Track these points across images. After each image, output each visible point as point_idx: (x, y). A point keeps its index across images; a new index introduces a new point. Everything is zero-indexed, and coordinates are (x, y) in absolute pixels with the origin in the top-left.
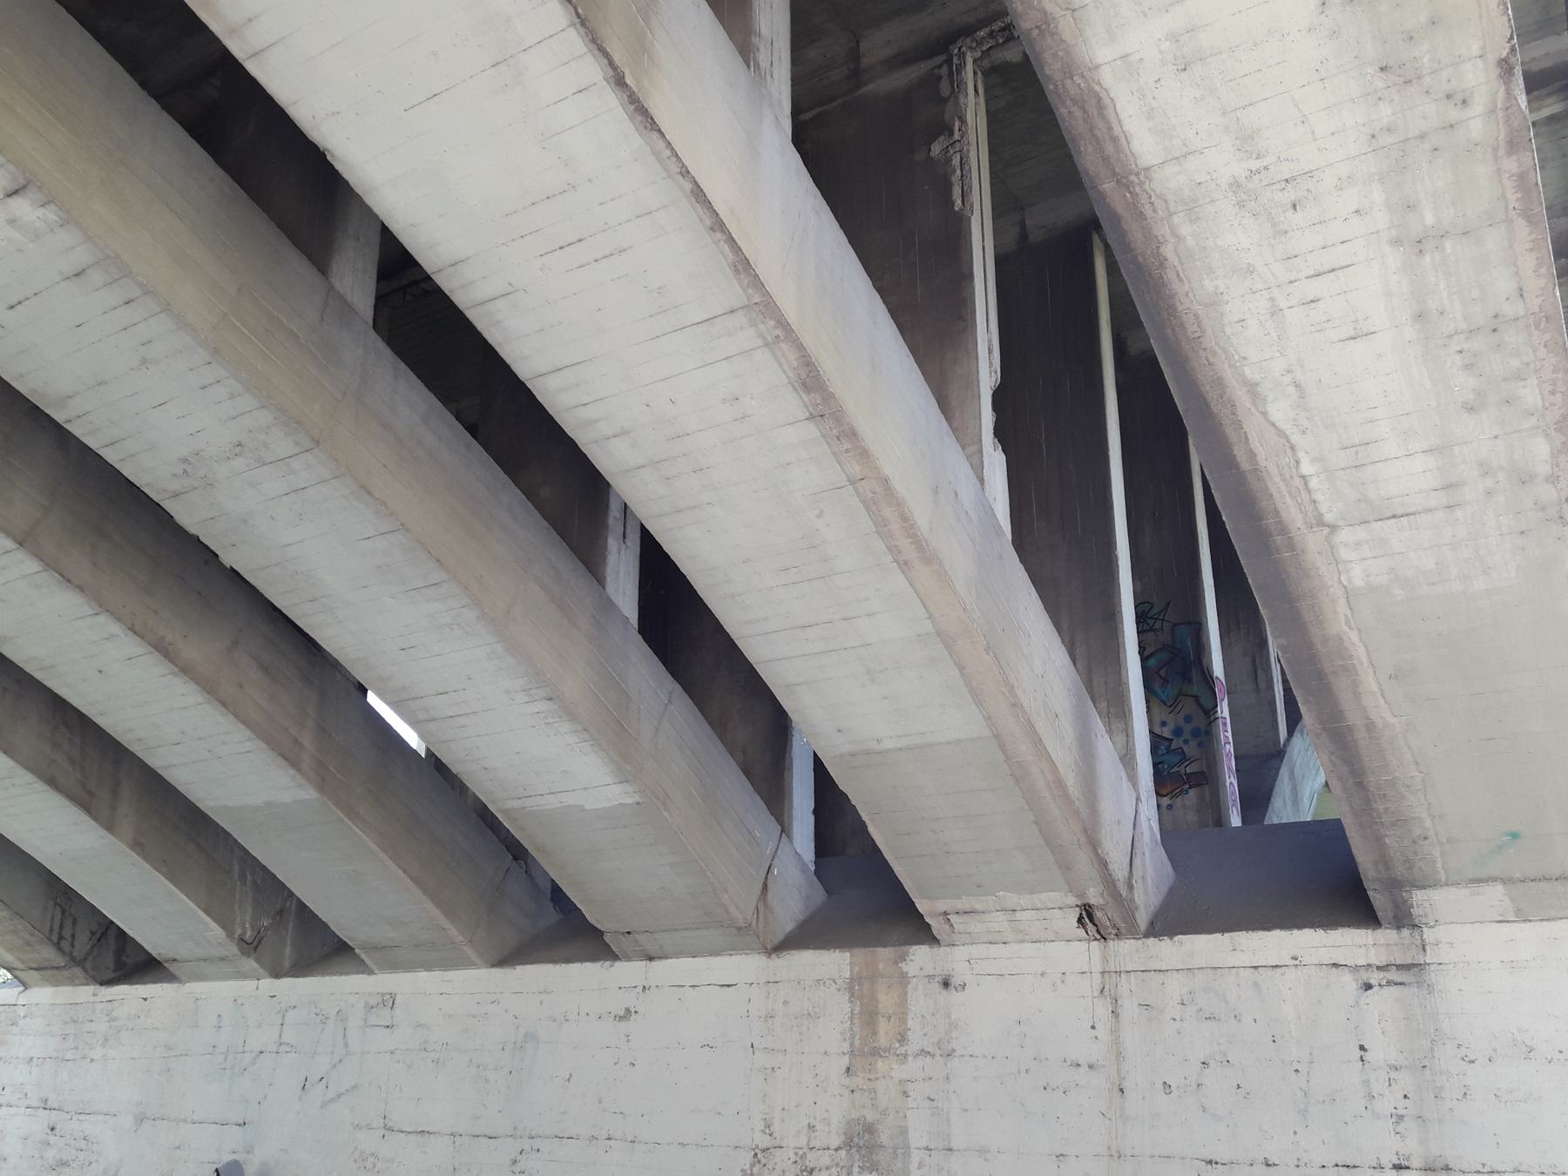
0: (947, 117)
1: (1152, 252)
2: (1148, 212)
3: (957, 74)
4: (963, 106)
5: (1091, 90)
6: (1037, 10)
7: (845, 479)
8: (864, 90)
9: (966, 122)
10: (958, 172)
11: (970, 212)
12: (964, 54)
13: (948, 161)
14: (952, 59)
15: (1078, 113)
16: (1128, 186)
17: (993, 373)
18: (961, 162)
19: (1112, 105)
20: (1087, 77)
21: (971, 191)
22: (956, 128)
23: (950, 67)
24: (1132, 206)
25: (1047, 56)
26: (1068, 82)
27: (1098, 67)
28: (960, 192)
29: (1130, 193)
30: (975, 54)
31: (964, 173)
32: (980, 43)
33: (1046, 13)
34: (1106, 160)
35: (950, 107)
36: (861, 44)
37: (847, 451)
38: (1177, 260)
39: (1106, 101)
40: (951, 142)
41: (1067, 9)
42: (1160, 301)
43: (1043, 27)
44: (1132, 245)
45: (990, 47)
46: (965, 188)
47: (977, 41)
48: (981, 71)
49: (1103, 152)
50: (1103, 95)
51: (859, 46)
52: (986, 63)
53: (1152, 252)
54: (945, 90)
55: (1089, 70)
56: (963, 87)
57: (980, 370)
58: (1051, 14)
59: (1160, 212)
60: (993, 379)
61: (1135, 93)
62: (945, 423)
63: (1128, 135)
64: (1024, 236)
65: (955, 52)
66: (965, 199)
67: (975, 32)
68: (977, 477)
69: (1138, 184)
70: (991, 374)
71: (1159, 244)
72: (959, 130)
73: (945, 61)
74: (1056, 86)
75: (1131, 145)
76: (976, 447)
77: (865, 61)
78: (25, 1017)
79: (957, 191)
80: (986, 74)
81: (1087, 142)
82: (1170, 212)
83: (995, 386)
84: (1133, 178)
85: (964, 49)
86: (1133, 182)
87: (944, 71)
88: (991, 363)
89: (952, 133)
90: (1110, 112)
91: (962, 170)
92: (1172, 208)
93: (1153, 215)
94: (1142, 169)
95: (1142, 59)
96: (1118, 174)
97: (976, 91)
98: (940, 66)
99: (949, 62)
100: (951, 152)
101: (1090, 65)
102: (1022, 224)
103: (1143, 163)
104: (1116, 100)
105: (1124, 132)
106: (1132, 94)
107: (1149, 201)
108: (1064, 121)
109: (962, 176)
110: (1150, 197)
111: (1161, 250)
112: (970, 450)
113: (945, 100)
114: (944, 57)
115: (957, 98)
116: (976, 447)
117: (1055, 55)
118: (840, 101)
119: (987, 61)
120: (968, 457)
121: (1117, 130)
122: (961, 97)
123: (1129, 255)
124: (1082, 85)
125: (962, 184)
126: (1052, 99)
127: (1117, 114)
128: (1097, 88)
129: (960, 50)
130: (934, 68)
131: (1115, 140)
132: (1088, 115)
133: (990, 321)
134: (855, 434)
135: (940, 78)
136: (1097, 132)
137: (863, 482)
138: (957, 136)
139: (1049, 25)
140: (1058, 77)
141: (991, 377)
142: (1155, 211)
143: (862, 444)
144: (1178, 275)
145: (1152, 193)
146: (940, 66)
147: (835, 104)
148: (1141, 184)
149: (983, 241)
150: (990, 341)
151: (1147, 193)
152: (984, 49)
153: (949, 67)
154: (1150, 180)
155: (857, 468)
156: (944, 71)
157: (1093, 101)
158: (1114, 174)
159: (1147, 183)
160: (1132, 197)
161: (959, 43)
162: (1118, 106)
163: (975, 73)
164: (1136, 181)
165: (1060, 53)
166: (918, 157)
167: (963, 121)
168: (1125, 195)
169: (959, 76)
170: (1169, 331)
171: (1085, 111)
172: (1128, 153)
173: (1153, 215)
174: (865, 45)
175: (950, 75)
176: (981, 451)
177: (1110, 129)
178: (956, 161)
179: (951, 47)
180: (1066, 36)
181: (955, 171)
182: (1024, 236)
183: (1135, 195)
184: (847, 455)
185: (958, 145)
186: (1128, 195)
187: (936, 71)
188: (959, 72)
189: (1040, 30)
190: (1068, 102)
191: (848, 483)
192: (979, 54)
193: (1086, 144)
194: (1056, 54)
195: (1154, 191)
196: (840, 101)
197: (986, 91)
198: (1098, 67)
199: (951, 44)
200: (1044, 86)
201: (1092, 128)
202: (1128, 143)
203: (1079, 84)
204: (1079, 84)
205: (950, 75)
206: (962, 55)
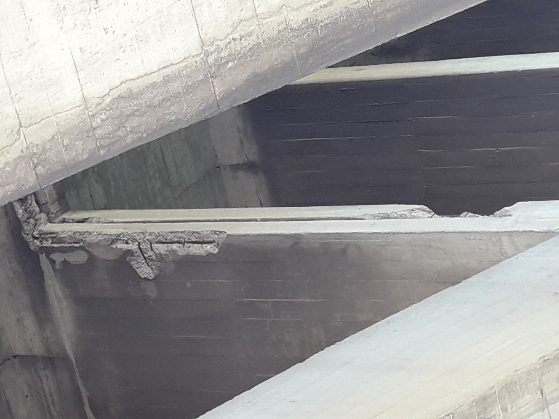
0: (110, 256)
1: (297, 37)
2: (251, 41)
3: (64, 243)
4: (100, 237)
5: (110, 107)
6: (16, 167)
7: (541, 413)
8: (70, 352)
9: (119, 235)
10: (175, 246)
11: (221, 236)
12: (41, 233)
13: (161, 258)
14: (46, 247)
15: (134, 122)
16: (220, 65)
17: (413, 214)
18: (164, 243)
19: (129, 82)
20: (95, 111)
21: (197, 233)
22: (125, 247)
23: (54, 250)
24: (243, 60)
25: (66, 157)
26: (99, 132)
27: (85, 99)
28: (196, 245)
29: (227, 62)
30: (43, 221)
31: (176, 240)
32: (31, 215)
33: (20, 157)
34: (188, 90)
35: (99, 253)
36: (18, 353)
37: (505, 410)
38: (307, 8)
39: (123, 90)
40: (139, 253)
41: (18, 133)
42: (355, 26)
43: (36, 161)
44: (287, 60)
45: (37, 202)
46: (194, 240)
47: (28, 218)
48: (62, 214)
49: (180, 93)
50: (115, 93)
51: (18, 356)
52: (54, 208)
53: (297, 37)
54: (79, 258)
55: (87, 109)
56: (78, 237)
57: (408, 231)
58: (22, 151)
59: (252, 28)
60: (421, 214)
61: (117, 57)
62: (473, 279)
63: (163, 65)
64: (250, 167)
65: (38, 243)
66: (206, 239)
67: (17, 218)
68: (544, 240)
69: (219, 53)
70: (414, 217)
71: (288, 29)
72: (127, 243)
73: (48, 256)
74: (102, 147)
75: (174, 62)
76: (504, 239)
77: (38, 349)
78: (88, 59)
79: (196, 250)
80: (66, 208)
81: (167, 112)
82: (252, 17)
83: (429, 212)
84: (211, 60)
85: (36, 233)
86: (215, 60)
87: (58, 257)
88: (401, 217)
89: (130, 253)
90: (135, 86)
91: (172, 243)
92: (249, 14)
93: (254, 37)
94: (202, 48)
95: (81, 49)
96: (206, 76)
97: (83, 221)
98: (53, 262)
99: (48, 251)
100: (150, 253)
101: (83, 107)
102: (235, 168)
103: (195, 48)
104: (123, 79)
105: (159, 70)
106: (117, 59)
107: (238, 41)
108: (140, 139)
109: (178, 242)
110: (234, 39)
111: (294, 26)
112: (507, 247)
113: (92, 259)
114: (43, 258)
115: (90, 244)
116: (504, 239)
117: (66, 147)
118: (80, 382)
119: (51, 207)
120: (518, 251)
121: (156, 78)
122: (89, 239)
123: (298, 63)
124: (103, 117)
125: (188, 242)
126: (116, 151)
127: (138, 78)
128: (108, 100)
129: (37, 238)
130: (53, 269)
131: (167, 80)
132: (137, 110)
133: (350, 215)
134: (484, 399)
135: (65, 262)
136: (156, 102)
137: (545, 391)
138: (133, 247)
139: (35, 154)
140: (91, 145)
141: (418, 217)
142: (250, 34)
143: (496, 389)
144: (326, 6)
145: (230, 37)
146: (53, 262)
147: (82, 389)
148: (219, 50)
149: (256, 220)
150: (374, 217)
151: (229, 43)
152: (37, 209)
153: (54, 252)
154: (215, 39)
155: (527, 397)
156: (58, 257)
157: (122, 104)
158: (204, 81)
159: (218, 43)
160: (233, 60)
161: (29, 238)
162: (131, 76)
163: (64, 221)
164: (214, 56)
165: (66, 142)
166: (152, 292)
167: (117, 238)
168: (230, 68)
169: (66, 239)
170: (389, 16)
171: (133, 114)
172: (183, 64)
173: (254, 37)
174: (20, 350)
175: (62, 250)
176: (510, 234)
177: (154, 85)
178: (162, 249)
179: (32, 248)
180: (47, 134)
181: (173, 251)
182: (250, 167)
183: (231, 57)
184: (510, 410)
185: (143, 246)
186: (230, 64)
187: (58, 267)
188: (61, 241)
189: (38, 164)
190: (119, 133)
191: (546, 410)
192: (43, 216)
193: (168, 114)
194: (67, 146)
195: (228, 35)
196: (80, 382)
197: (84, 208)
198: (85, 99)
199: (28, 247)
200: (100, 161)
201: (152, 107)
202: (172, 64)
203: (102, 120)
204: (102, 120)
205: (62, 250)
206: (43, 236)
